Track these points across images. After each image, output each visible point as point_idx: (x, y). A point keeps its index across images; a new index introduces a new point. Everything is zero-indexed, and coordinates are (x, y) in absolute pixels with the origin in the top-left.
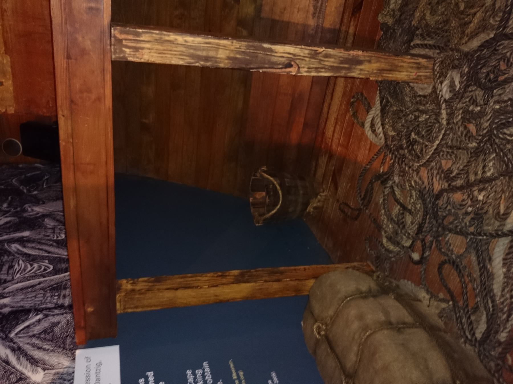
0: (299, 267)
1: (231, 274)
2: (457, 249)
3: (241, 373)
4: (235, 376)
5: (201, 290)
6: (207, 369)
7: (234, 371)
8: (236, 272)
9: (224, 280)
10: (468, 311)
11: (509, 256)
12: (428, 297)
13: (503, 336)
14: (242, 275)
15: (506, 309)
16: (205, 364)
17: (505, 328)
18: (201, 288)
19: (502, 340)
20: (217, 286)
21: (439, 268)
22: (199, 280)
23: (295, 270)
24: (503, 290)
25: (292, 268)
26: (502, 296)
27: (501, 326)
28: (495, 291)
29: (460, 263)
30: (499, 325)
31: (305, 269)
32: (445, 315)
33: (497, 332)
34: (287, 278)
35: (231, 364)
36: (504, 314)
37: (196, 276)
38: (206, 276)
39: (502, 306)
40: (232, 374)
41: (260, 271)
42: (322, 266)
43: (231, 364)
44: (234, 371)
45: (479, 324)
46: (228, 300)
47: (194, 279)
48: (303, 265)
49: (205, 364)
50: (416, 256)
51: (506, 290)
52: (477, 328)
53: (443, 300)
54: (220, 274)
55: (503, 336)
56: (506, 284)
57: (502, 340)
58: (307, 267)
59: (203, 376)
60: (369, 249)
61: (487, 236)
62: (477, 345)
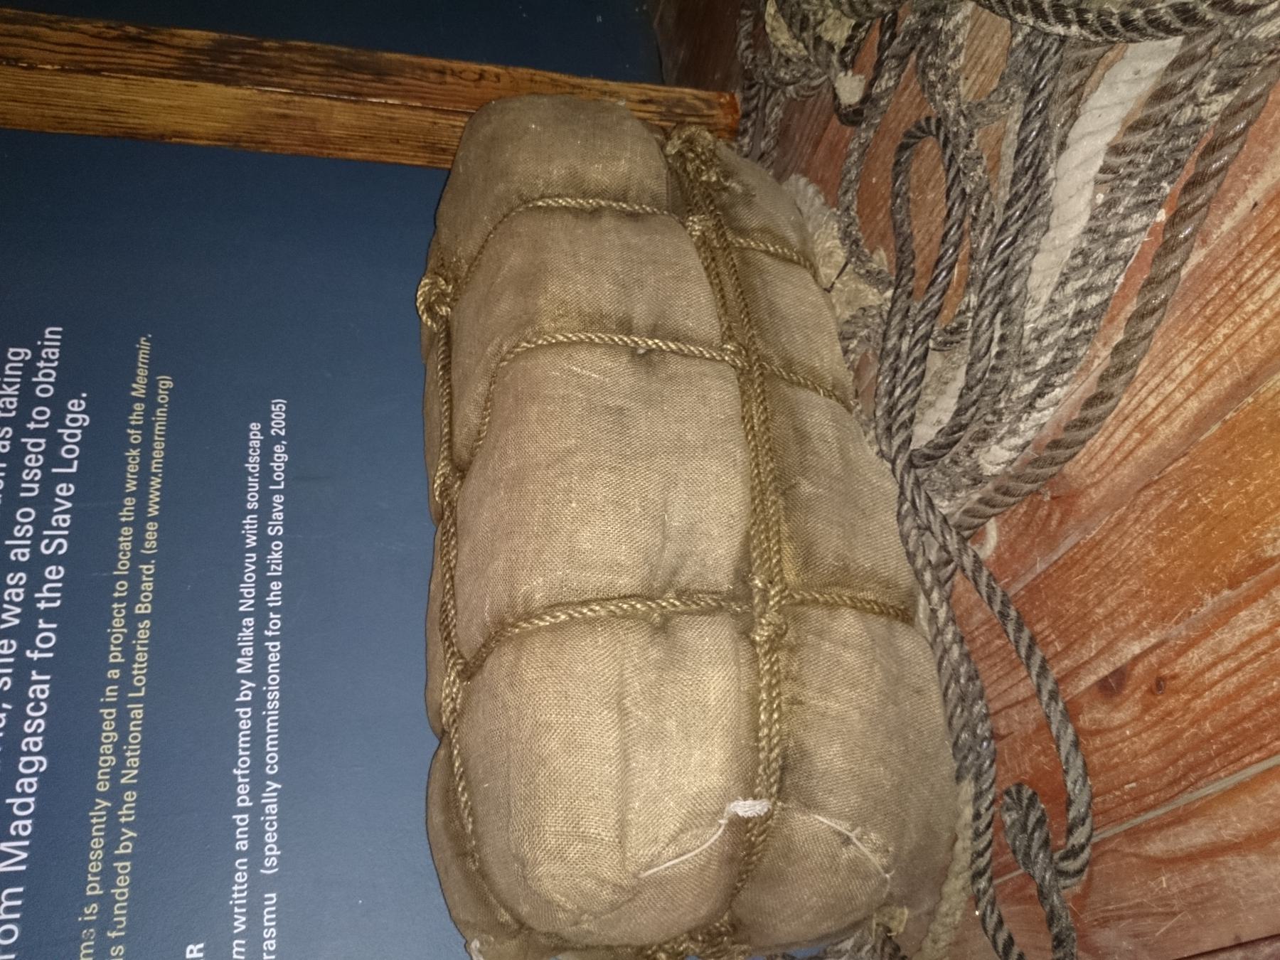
0: (457, 65)
1: (176, 41)
2: (982, 78)
3: (166, 383)
4: (139, 389)
5: (35, 75)
6: (52, 352)
7: (142, 372)
8: (200, 37)
9: (137, 58)
10: (927, 336)
11: (1142, 137)
12: (840, 256)
13: (995, 458)
14: (218, 52)
15: (1044, 361)
16: (52, 334)
17: (1013, 432)
18: (31, 67)
19: (989, 470)
20: (96, 72)
21: (903, 148)
22: (35, 38)
23: (442, 72)
24: (1062, 284)
25: (436, 62)
26: (1052, 305)
27: (1006, 419)
28: (1034, 281)
29: (963, 139)
30: (998, 414)
31: (482, 76)
32: (864, 333)
33: (983, 437)
34: (391, 97)
35: (144, 347)
36: (1030, 376)
37: (35, 22)
38: (72, 30)
39: (1034, 345)
40: (133, 377)
41: (299, 49)
42: (556, 76)
43: (144, 347)
44: (142, 372)
45: (942, 393)
46: (162, 136)
47: (18, 28)
48: (479, 60)
49: (52, 334)
50: (850, 88)
51: (1070, 288)
52: (931, 405)
53: (873, 278)
54: (132, 30)
55: (995, 458)
56: (1079, 260)
57: (989, 470)
58: (491, 69)
59: (29, 369)
60: (744, 44)
61: (1083, 23)
62: (900, 462)
